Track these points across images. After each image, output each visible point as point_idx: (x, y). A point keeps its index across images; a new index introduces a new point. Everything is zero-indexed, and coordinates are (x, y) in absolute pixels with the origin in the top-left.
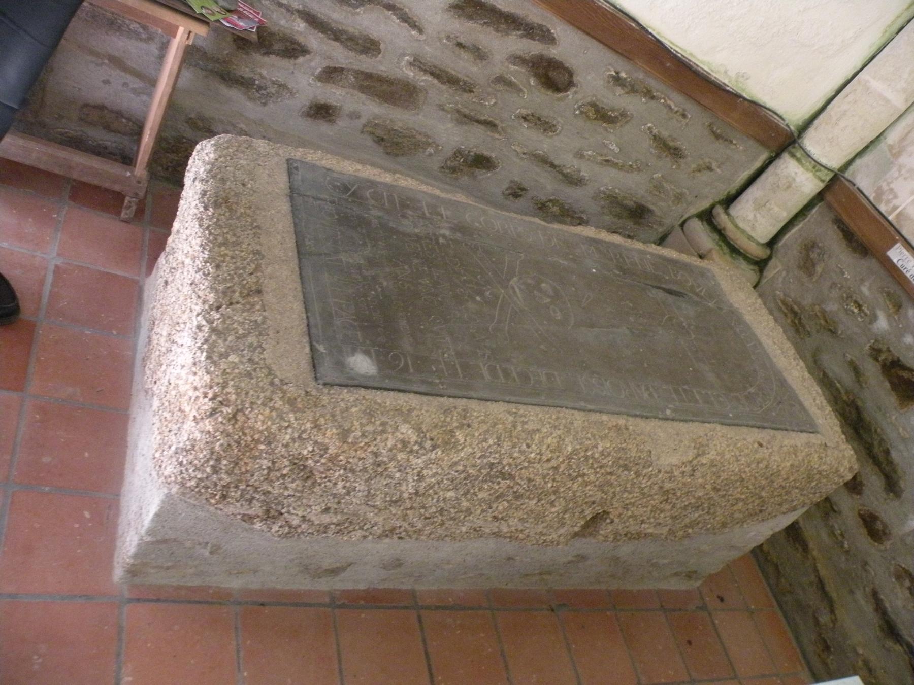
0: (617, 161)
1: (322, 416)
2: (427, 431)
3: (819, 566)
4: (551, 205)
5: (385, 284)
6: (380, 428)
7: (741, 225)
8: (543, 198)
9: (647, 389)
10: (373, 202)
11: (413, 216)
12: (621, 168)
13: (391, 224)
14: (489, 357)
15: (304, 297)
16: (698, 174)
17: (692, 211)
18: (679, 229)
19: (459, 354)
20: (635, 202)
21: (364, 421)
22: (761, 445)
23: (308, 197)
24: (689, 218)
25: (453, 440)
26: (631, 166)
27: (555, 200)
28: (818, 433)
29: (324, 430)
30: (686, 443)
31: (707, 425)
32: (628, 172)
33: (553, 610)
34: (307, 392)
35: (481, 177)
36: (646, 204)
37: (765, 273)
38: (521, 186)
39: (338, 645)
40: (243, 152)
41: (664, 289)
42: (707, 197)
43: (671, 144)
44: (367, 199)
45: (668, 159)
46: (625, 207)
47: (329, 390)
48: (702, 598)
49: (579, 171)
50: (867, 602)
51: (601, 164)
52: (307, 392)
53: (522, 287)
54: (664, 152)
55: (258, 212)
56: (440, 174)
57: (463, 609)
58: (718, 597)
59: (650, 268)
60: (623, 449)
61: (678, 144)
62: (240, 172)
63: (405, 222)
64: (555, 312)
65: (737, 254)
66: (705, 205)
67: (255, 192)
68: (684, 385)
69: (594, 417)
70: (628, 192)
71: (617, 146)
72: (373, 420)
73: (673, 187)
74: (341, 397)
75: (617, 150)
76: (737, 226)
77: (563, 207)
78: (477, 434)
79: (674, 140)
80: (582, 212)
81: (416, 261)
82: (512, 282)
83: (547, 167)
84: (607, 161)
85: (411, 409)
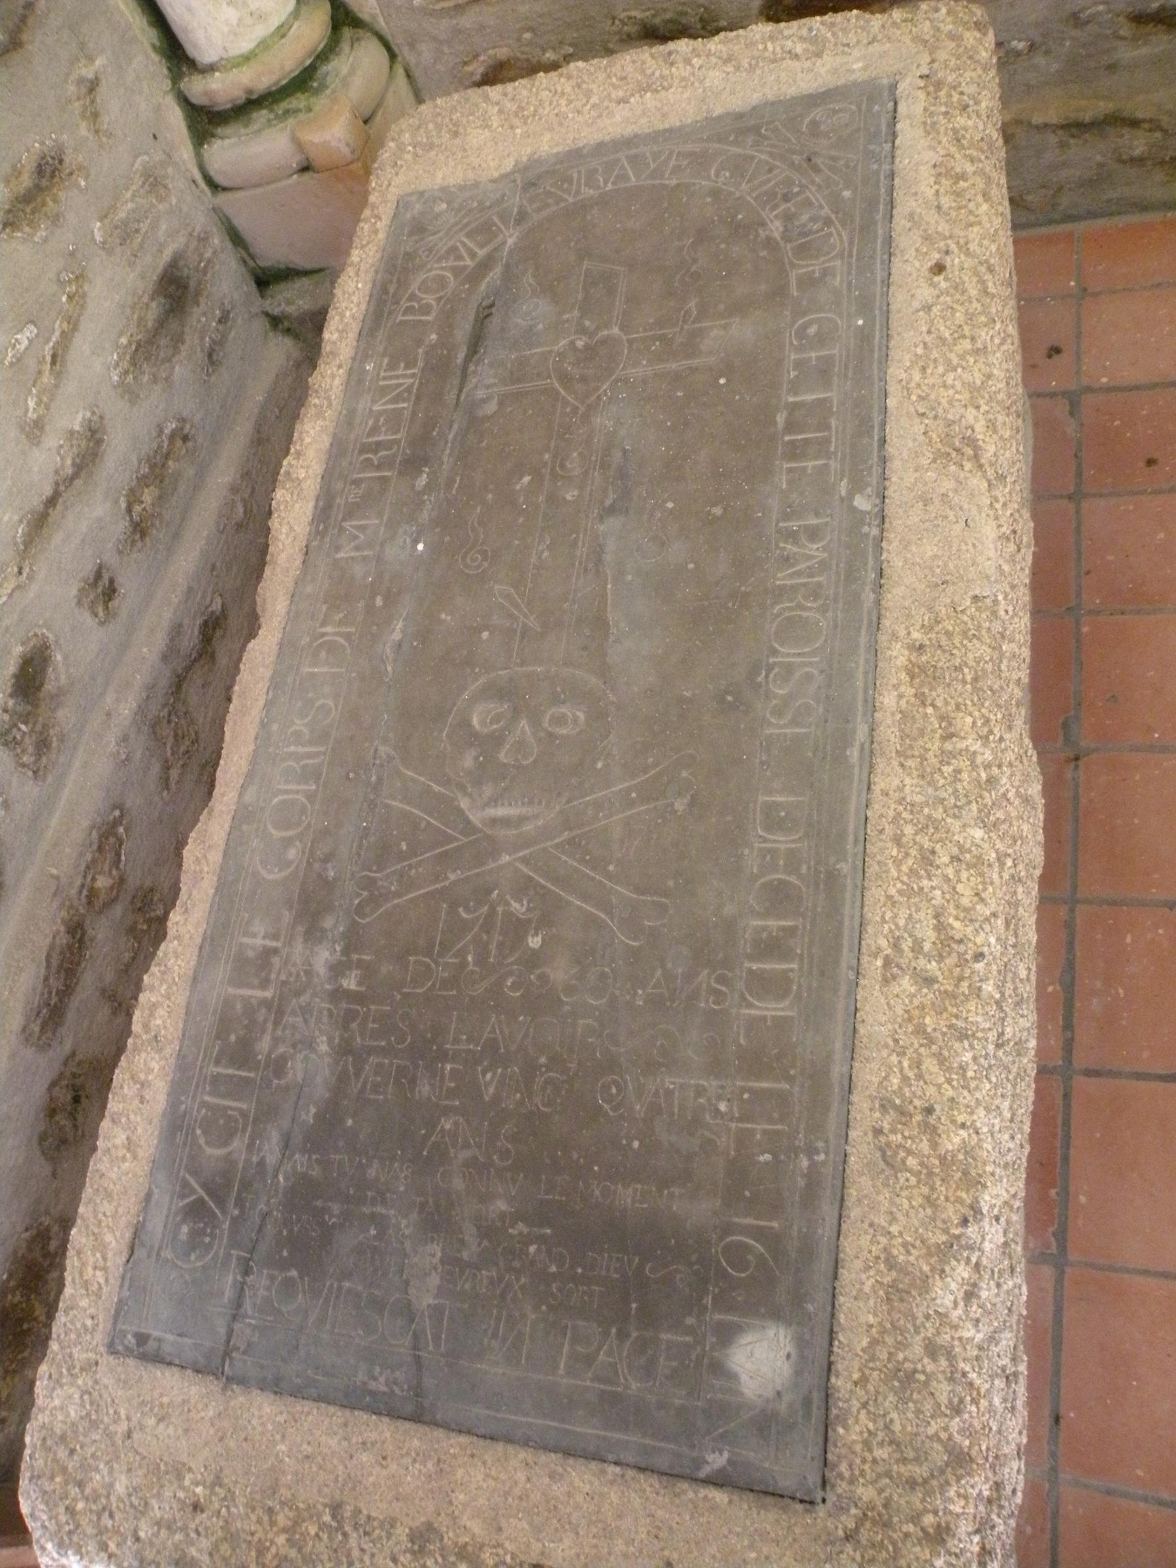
0: (57, 334)
1: (915, 1519)
2: (946, 1231)
3: (1037, 119)
4: (137, 508)
5: (502, 1205)
6: (944, 1363)
7: (245, 45)
8: (123, 525)
9: (792, 536)
10: (238, 1144)
11: (276, 1041)
12: (73, 324)
13: (309, 1115)
14: (722, 980)
15: (554, 1450)
16: (105, 119)
17: (185, 156)
18: (222, 199)
19: (716, 1067)
20: (152, 299)
21: (928, 1407)
22: (939, 268)
23: (230, 1333)
24: (202, 168)
25: (961, 1157)
26: (70, 298)
27: (127, 496)
28: (893, 87)
29: (949, 1518)
30: (948, 485)
31: (891, 402)
32: (83, 307)
33: (1077, 759)
34: (847, 1538)
35: (63, 677)
36: (160, 269)
37: (364, 16)
38: (91, 580)
39: (1146, 1272)
40: (84, 1467)
41: (468, 359)
42: (158, 109)
43: (26, 181)
44: (229, 1160)
45: (62, 195)
46: (161, 323)
47: (840, 1476)
48: (1052, 395)
49: (72, 433)
50: (1145, 44)
51: (58, 375)
52: (847, 1538)
53: (488, 790)
54: (44, 204)
55: (285, 1493)
56: (50, 778)
57: (1070, 965)
58: (1050, 356)
59: (407, 377)
60: (976, 679)
61: (28, 162)
62: (154, 1503)
63: (296, 1070)
64: (560, 720)
65: (311, 78)
66: (176, 117)
67: (218, 1481)
68: (774, 423)
69: (889, 734)
70: (128, 311)
71: (20, 331)
72: (922, 1378)
73: (129, 195)
74: (858, 1448)
75: (30, 331)
76: (247, 58)
77: (145, 477)
78: (950, 1093)
79: (17, 172)
80: (161, 432)
81: (424, 1089)
82: (475, 818)
83: (55, 514)
84: (54, 357)
85: (887, 1260)
